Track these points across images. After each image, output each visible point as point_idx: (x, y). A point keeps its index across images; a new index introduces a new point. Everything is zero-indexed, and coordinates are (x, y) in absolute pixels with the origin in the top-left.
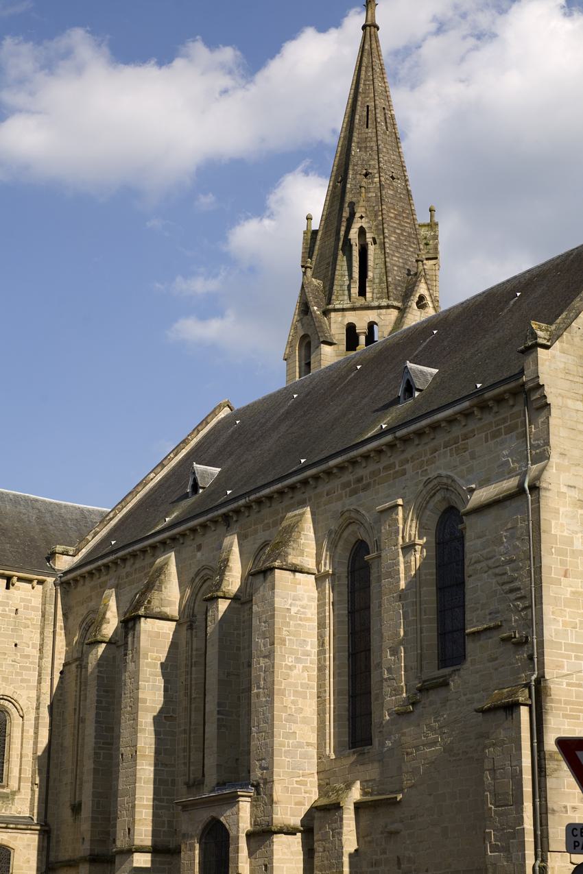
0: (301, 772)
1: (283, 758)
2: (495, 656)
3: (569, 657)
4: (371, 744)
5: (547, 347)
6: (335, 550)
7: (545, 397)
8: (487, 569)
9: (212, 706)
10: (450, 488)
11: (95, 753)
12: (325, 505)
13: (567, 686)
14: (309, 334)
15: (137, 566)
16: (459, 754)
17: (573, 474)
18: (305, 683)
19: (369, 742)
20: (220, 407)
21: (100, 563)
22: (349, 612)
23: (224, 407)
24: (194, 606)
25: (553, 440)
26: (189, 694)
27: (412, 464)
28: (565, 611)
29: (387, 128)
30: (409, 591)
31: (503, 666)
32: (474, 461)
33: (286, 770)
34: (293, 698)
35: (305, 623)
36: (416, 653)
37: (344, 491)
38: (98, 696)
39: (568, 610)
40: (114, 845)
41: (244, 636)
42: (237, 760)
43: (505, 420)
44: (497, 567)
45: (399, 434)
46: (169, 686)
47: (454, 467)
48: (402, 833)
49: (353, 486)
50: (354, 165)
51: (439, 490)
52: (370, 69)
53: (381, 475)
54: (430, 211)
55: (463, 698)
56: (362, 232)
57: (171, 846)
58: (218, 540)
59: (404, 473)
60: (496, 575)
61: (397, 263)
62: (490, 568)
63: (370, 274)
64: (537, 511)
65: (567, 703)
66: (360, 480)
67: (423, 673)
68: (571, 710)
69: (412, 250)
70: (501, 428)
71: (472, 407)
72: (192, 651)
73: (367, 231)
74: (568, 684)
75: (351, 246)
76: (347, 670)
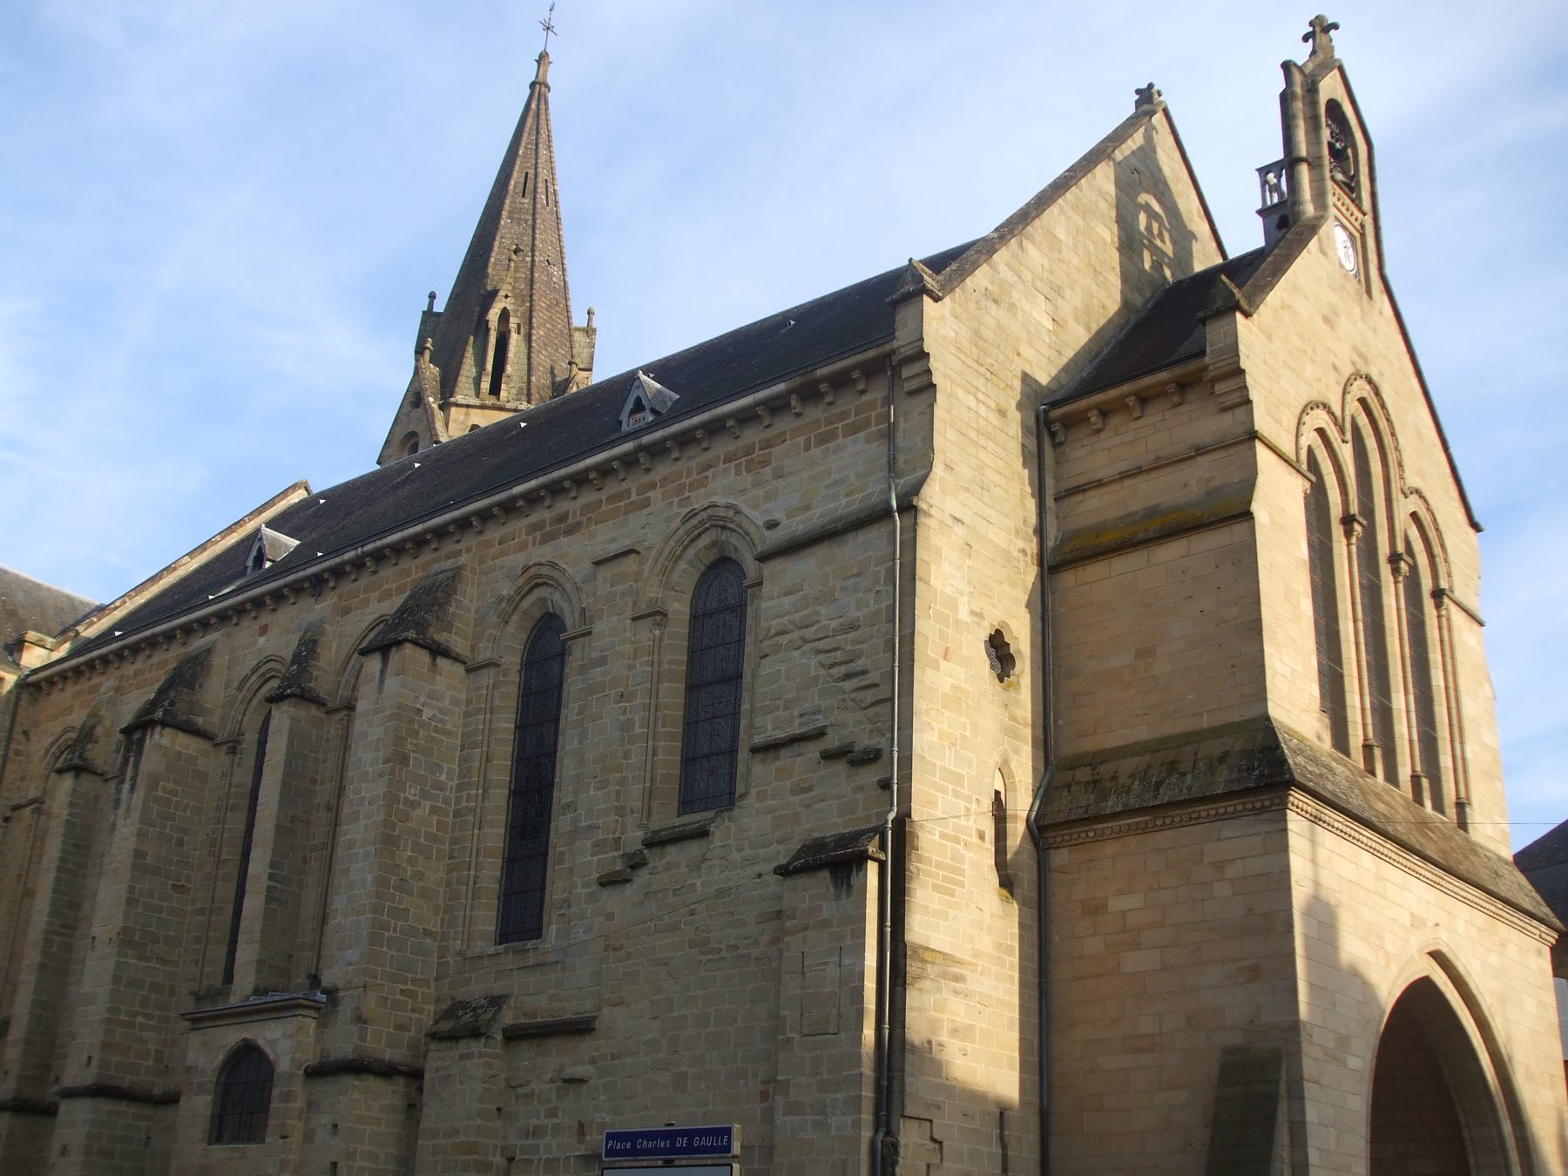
0: (410, 976)
1: (385, 949)
2: (809, 784)
3: (944, 791)
4: (539, 936)
5: (937, 299)
6: (504, 627)
7: (929, 372)
8: (799, 643)
9: (259, 864)
10: (729, 525)
11: (46, 940)
12: (494, 559)
13: (940, 838)
14: (418, 431)
15: (155, 660)
16: (720, 950)
17: (961, 502)
18: (432, 833)
19: (537, 932)
20: (294, 487)
21: (95, 654)
22: (516, 728)
23: (300, 488)
24: (242, 719)
25: (938, 442)
26: (217, 852)
27: (662, 490)
28: (943, 714)
29: (547, 203)
30: (638, 687)
31: (823, 800)
32: (780, 480)
33: (387, 969)
34: (410, 854)
35: (442, 738)
36: (642, 786)
37: (530, 537)
38: (63, 851)
39: (947, 713)
40: (1200, 327)
41: (325, 761)
42: (290, 956)
43: (844, 415)
44: (820, 639)
45: (646, 439)
46: (186, 838)
47: (741, 491)
48: (592, 1082)
49: (548, 529)
50: (502, 237)
51: (707, 529)
52: (534, 132)
53: (603, 508)
54: (589, 313)
55: (736, 856)
56: (505, 315)
57: (155, 1092)
58: (298, 618)
59: (646, 503)
60: (819, 652)
61: (544, 363)
62: (805, 641)
63: (509, 369)
64: (910, 545)
65: (939, 866)
66: (563, 518)
67: (651, 819)
68: (945, 879)
69: (563, 352)
70: (837, 428)
71: (789, 392)
72: (230, 788)
73: (511, 313)
74: (943, 836)
75: (488, 330)
76: (504, 817)
